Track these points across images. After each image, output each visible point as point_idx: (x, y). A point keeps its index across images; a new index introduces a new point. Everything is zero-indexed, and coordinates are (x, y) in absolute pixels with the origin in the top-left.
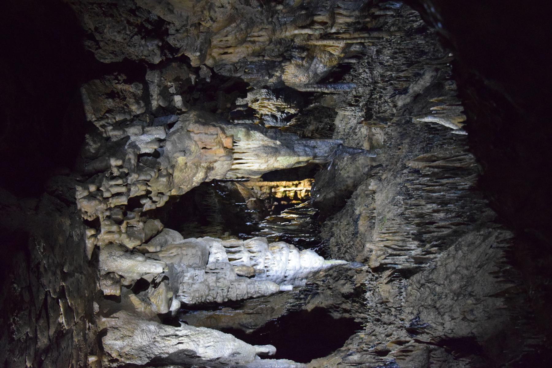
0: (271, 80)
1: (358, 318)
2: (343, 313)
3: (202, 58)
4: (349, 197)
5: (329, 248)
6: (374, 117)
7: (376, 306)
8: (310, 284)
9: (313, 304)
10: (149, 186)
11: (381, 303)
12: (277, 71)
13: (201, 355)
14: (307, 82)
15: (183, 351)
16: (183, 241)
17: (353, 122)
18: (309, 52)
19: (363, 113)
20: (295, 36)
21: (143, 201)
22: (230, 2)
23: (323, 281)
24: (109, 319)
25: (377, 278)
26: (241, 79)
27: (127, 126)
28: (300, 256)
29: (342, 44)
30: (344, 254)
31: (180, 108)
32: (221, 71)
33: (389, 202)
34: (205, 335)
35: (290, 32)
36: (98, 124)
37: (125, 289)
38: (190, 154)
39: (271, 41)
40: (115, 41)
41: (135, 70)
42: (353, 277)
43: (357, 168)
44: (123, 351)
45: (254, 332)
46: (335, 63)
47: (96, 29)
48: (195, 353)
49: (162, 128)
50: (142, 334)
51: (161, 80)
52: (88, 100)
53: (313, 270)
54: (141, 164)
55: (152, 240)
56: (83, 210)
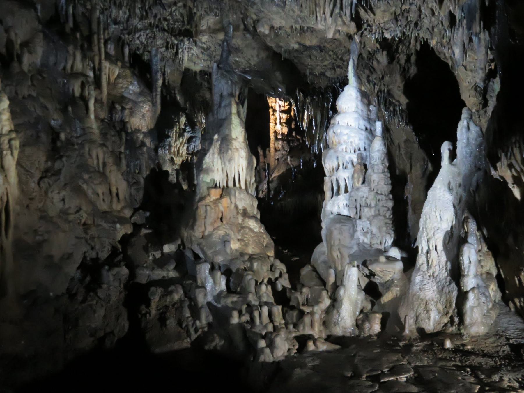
0: (148, 144)
1: (415, 46)
2: (410, 63)
3: (122, 221)
4: (280, 55)
5: (338, 78)
6: (188, 27)
7: (400, 26)
8: (378, 100)
9: (400, 96)
10: (263, 281)
11: (397, 21)
12: (137, 137)
13: (450, 225)
14: (150, 103)
15: (445, 245)
16: (324, 243)
17: (195, 50)
18: (116, 102)
19: (186, 39)
20: (97, 117)
21: (280, 288)
22: (57, 191)
23: (374, 85)
24: (407, 326)
25: (369, 25)
26: (147, 177)
27: (196, 304)
28: (344, 113)
29: (106, 65)
30: (344, 61)
31: (177, 246)
32: (138, 200)
33: (283, 10)
34: (428, 221)
35: (93, 122)
36: (194, 336)
37: (376, 308)
38: (228, 235)
39: (103, 145)
40: (104, 314)
41: (136, 294)
42: (369, 52)
43: (247, 46)
44: (442, 310)
45: (431, 162)
46: (128, 72)
47: (92, 335)
48: (447, 232)
49: (198, 267)
50: (425, 290)
51: (146, 267)
52: (169, 345)
53: (359, 98)
54: (239, 289)
55: (323, 278)
56: (286, 354)
